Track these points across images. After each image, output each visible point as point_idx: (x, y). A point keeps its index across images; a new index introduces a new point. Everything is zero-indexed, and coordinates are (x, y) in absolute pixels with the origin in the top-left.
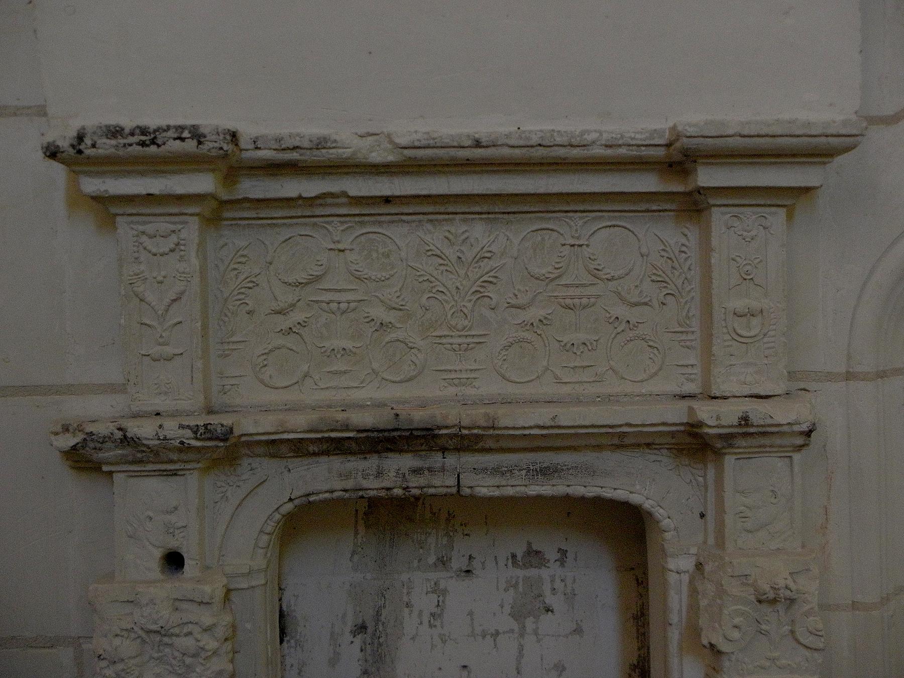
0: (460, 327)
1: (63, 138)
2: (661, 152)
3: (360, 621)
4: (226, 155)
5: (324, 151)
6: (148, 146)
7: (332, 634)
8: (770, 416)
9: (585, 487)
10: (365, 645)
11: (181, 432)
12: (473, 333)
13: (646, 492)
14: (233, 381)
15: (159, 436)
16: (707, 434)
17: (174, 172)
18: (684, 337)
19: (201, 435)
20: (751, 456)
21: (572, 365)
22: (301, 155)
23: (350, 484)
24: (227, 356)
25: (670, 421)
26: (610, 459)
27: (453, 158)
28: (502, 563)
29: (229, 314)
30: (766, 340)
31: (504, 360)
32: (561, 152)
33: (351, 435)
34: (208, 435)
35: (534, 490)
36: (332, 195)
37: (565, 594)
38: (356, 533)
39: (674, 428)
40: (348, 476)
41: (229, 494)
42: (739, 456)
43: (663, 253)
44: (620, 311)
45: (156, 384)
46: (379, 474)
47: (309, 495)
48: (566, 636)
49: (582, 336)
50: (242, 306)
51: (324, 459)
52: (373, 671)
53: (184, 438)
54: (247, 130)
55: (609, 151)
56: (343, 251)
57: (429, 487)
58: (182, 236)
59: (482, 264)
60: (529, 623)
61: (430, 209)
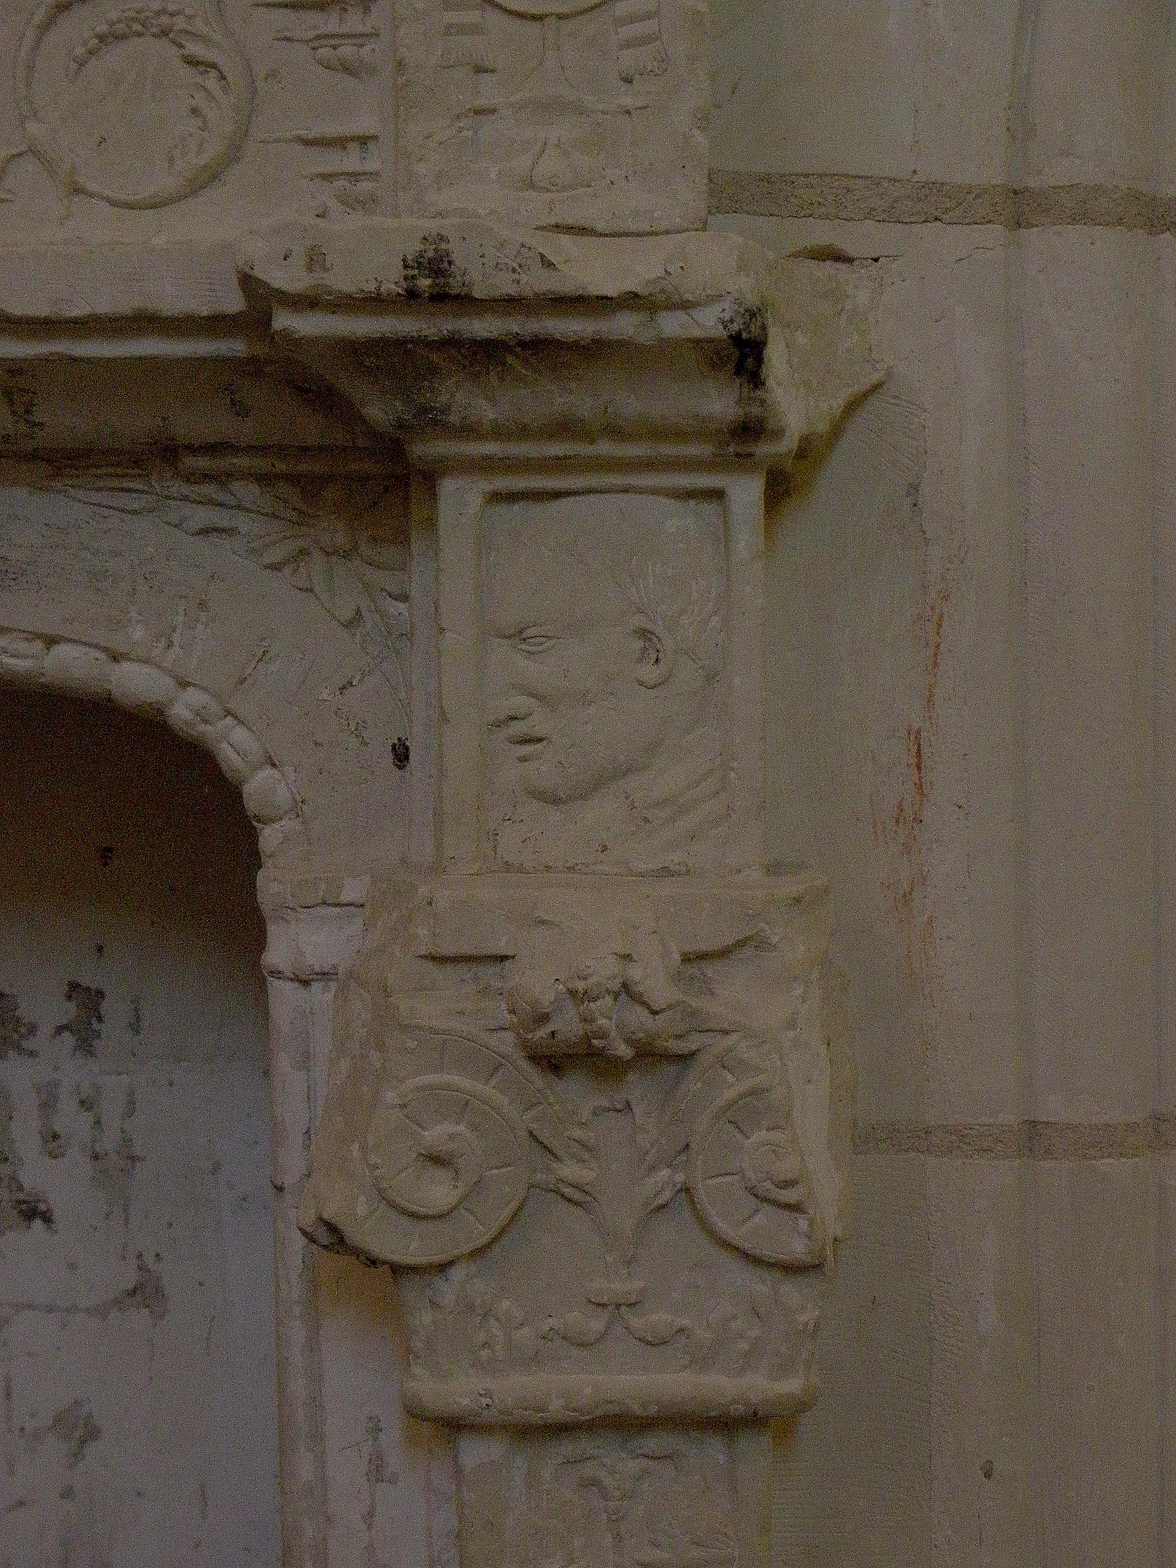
8: (542, 256)
13: (172, 654)
16: (296, 342)
37: (96, 1157)
39: (202, 347)
42: (504, 483)
48: (100, 1311)
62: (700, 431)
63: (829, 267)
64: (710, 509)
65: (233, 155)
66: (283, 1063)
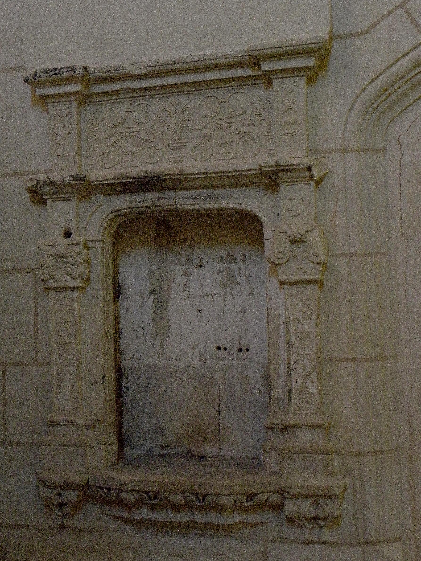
0: (176, 139)
1: (29, 74)
2: (247, 58)
4: (83, 76)
5: (119, 71)
6: (57, 75)
7: (140, 294)
9: (228, 204)
11: (69, 178)
12: (182, 141)
14: (90, 166)
17: (67, 84)
18: (269, 137)
20: (291, 184)
21: (222, 152)
22: (111, 74)
23: (133, 205)
24: (88, 157)
25: (253, 168)
26: (237, 192)
27: (166, 70)
28: (216, 261)
29: (89, 140)
30: (298, 134)
31: (195, 152)
32: (207, 62)
33: (130, 180)
35: (207, 206)
36: (125, 89)
37: (246, 276)
40: (133, 202)
41: (88, 210)
43: (260, 102)
44: (243, 128)
46: (145, 201)
47: (118, 210)
48: (246, 296)
49: (226, 140)
50: (94, 137)
51: (123, 195)
54: (91, 66)
55: (226, 60)
56: (131, 112)
57: (165, 205)
58: (71, 109)
59: (184, 113)
60: (229, 290)
61: (163, 92)
62: (306, 177)
63: (323, 159)
64: (309, 185)
65: (259, 152)
66: (266, 249)
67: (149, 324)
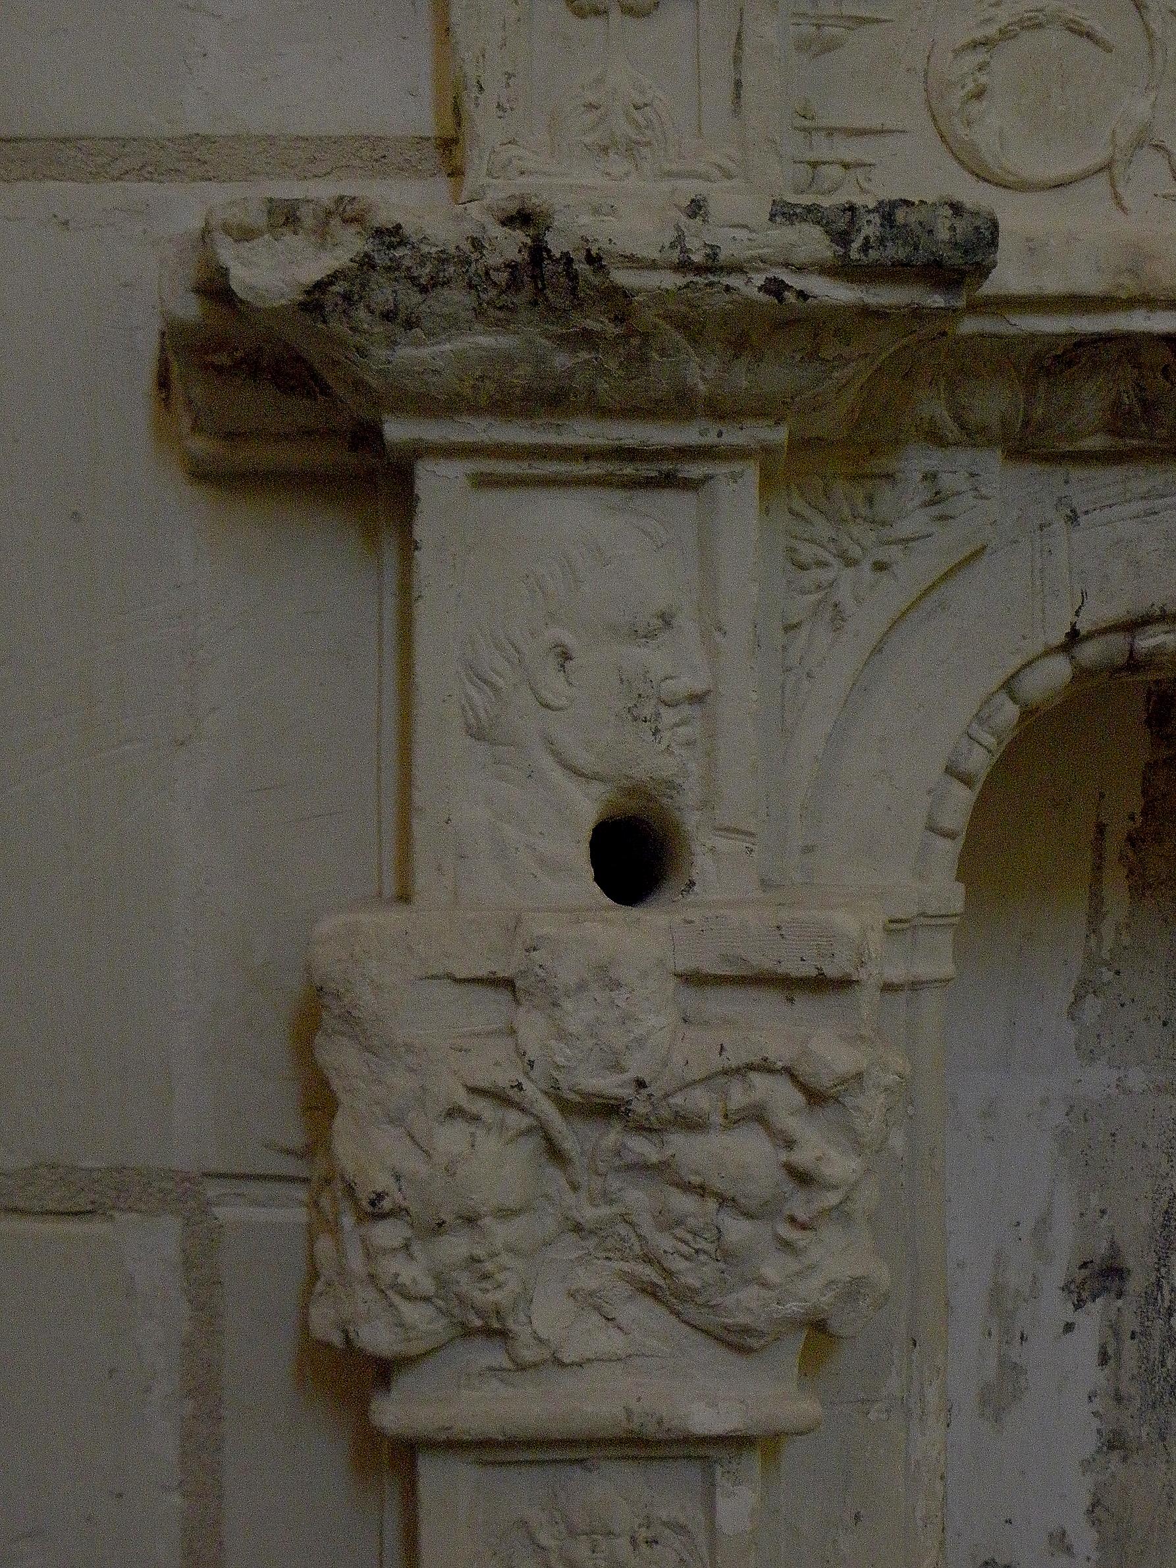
3: (1103, 1248)
7: (997, 1292)
10: (1116, 1334)
14: (850, 150)
15: (684, 251)
19: (866, 247)
24: (830, 47)
34: (896, 252)
38: (1096, 914)
45: (592, 107)
52: (1145, 1438)
53: (786, 265)
67: (1060, 1542)
